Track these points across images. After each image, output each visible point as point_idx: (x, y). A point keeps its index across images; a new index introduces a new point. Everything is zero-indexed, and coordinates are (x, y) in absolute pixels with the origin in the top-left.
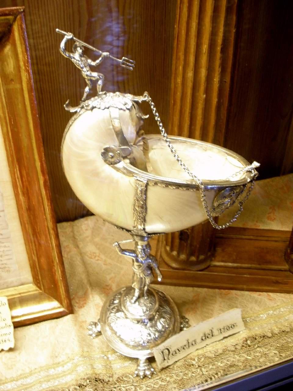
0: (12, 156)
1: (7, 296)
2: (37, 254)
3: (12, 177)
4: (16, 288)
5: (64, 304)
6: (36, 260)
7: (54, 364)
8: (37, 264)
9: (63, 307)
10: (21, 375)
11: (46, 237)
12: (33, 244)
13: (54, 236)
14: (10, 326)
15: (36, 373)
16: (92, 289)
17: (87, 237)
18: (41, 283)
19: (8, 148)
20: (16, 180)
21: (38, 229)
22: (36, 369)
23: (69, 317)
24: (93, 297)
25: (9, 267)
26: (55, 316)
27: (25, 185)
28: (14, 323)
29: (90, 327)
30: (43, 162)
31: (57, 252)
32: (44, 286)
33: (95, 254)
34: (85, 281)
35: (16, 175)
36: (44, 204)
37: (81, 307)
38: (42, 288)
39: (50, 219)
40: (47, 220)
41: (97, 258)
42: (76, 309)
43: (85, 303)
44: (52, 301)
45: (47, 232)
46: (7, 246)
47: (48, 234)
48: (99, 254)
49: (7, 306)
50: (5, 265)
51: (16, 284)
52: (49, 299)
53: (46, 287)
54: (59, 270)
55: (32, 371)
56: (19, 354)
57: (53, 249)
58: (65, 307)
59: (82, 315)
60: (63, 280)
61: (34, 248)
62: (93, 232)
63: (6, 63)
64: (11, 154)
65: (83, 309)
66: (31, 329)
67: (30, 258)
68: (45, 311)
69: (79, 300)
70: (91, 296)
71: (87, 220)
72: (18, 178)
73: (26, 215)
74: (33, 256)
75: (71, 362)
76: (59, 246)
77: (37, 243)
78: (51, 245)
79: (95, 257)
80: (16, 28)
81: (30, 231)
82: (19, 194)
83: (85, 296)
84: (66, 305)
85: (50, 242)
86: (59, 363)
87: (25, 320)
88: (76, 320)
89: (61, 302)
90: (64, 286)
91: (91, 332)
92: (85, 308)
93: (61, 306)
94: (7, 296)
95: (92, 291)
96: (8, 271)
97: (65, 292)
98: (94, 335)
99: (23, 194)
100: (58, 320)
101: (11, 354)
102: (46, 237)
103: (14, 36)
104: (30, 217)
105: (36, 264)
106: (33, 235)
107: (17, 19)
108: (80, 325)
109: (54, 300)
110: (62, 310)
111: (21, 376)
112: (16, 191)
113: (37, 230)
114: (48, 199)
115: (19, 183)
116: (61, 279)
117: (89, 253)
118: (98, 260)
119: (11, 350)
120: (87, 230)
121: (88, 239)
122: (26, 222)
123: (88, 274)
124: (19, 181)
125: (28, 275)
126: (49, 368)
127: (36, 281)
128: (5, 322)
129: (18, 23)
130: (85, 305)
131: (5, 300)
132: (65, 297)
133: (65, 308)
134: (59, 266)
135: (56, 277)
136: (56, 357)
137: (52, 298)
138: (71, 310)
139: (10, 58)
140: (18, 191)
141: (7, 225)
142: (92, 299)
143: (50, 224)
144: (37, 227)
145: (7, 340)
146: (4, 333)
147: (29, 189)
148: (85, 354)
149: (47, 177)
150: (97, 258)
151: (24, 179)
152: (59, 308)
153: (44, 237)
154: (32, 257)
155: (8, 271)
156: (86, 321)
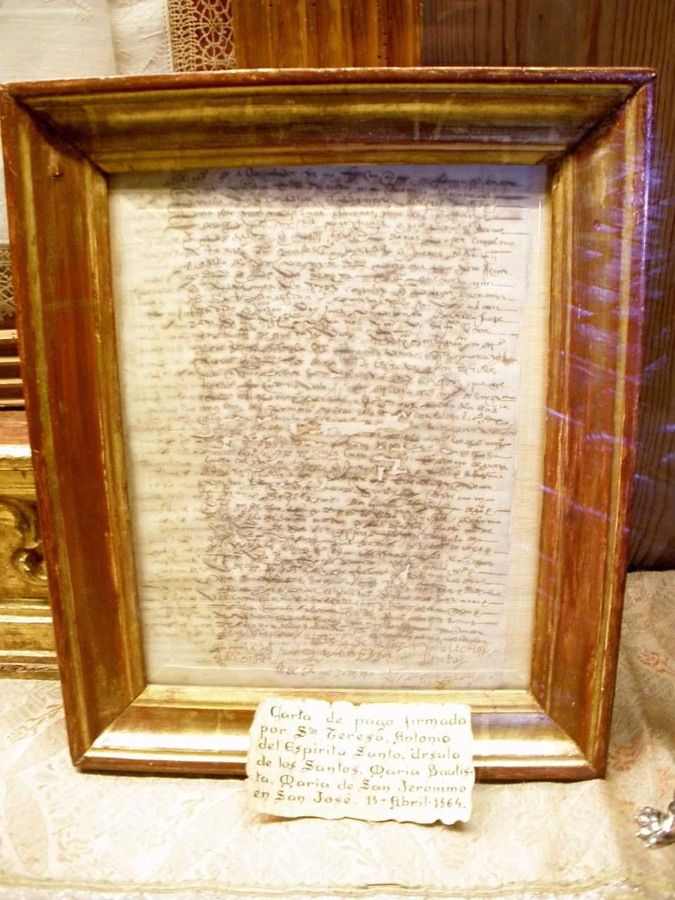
0: (560, 391)
1: (473, 707)
2: (560, 623)
3: (548, 436)
4: (488, 692)
5: (590, 751)
6: (554, 637)
7: (554, 884)
8: (553, 647)
9: (586, 758)
10: (477, 888)
11: (594, 587)
12: (558, 598)
13: (616, 587)
14: (467, 772)
15: (512, 892)
16: (653, 732)
17: (640, 615)
18: (549, 690)
19: (555, 371)
20: (557, 447)
21: (577, 567)
22: (513, 883)
23: (595, 784)
24: (654, 751)
25: (485, 642)
26: (562, 775)
27: (575, 462)
28: (477, 769)
29: (644, 819)
30: (634, 415)
31: (610, 627)
32: (552, 700)
33: (656, 657)
34: (637, 712)
35: (560, 434)
36: (612, 510)
37: (622, 769)
38: (548, 703)
39: (617, 545)
40: (607, 548)
41: (660, 666)
42: (610, 770)
43: (633, 762)
44: (563, 738)
45: (601, 576)
46: (494, 592)
47: (602, 581)
48: (667, 659)
49: (469, 725)
50: (478, 635)
51: (490, 683)
52: (557, 735)
53: (558, 704)
54: (604, 668)
55: (502, 886)
56: (475, 840)
57: (603, 617)
58: (590, 758)
59: (623, 786)
60: (605, 692)
61: (557, 607)
62: (652, 607)
63: (590, 185)
64: (559, 387)
65: (625, 774)
66: (506, 791)
67: (539, 629)
68: (542, 757)
69: (618, 752)
70: (649, 748)
71: (639, 578)
72: (563, 444)
73: (558, 528)
74: (550, 626)
75: (597, 890)
76: (618, 613)
77: (566, 597)
78: (601, 606)
79: (657, 663)
80: (631, 110)
81: (559, 565)
82: (556, 478)
83: (634, 747)
84: (595, 754)
85: (601, 601)
86: (567, 885)
87: (494, 769)
88: (611, 797)
89: (582, 743)
90: (603, 708)
91: (645, 832)
92: (631, 771)
93: (582, 754)
94: (473, 707)
95: (652, 737)
96: (482, 651)
97: (602, 722)
98: (653, 840)
99: (566, 480)
100: (568, 786)
101: (454, 836)
102: (594, 587)
103: (623, 127)
104: (567, 536)
105: (549, 647)
106: (564, 577)
107: (638, 93)
108: (621, 808)
109: (566, 736)
110: (581, 763)
111: (478, 891)
112: (551, 471)
113: (575, 568)
114: (623, 500)
115: (562, 455)
116: (602, 689)
117: (643, 651)
118: (663, 670)
119: (457, 826)
120: (639, 599)
121: (641, 621)
122: (555, 545)
123: (643, 700)
124: (563, 449)
125: (520, 670)
126: (547, 890)
127: (539, 684)
128: (459, 761)
129: (638, 101)
130: (631, 766)
131: (466, 713)
132: (598, 733)
133: (590, 763)
134: (607, 660)
135: (591, 684)
136: (561, 869)
137: (563, 732)
138: (599, 771)
139: (603, 174)
140: (554, 472)
141: (509, 545)
142: (650, 756)
143: (613, 558)
144: (578, 562)
145: (453, 802)
146: (436, 786)
147: (582, 471)
148: (633, 878)
149: (633, 447)
150: (660, 666)
151: (576, 447)
152: (576, 757)
153: (587, 587)
154: (546, 626)
155: (482, 651)
156: (632, 803)
